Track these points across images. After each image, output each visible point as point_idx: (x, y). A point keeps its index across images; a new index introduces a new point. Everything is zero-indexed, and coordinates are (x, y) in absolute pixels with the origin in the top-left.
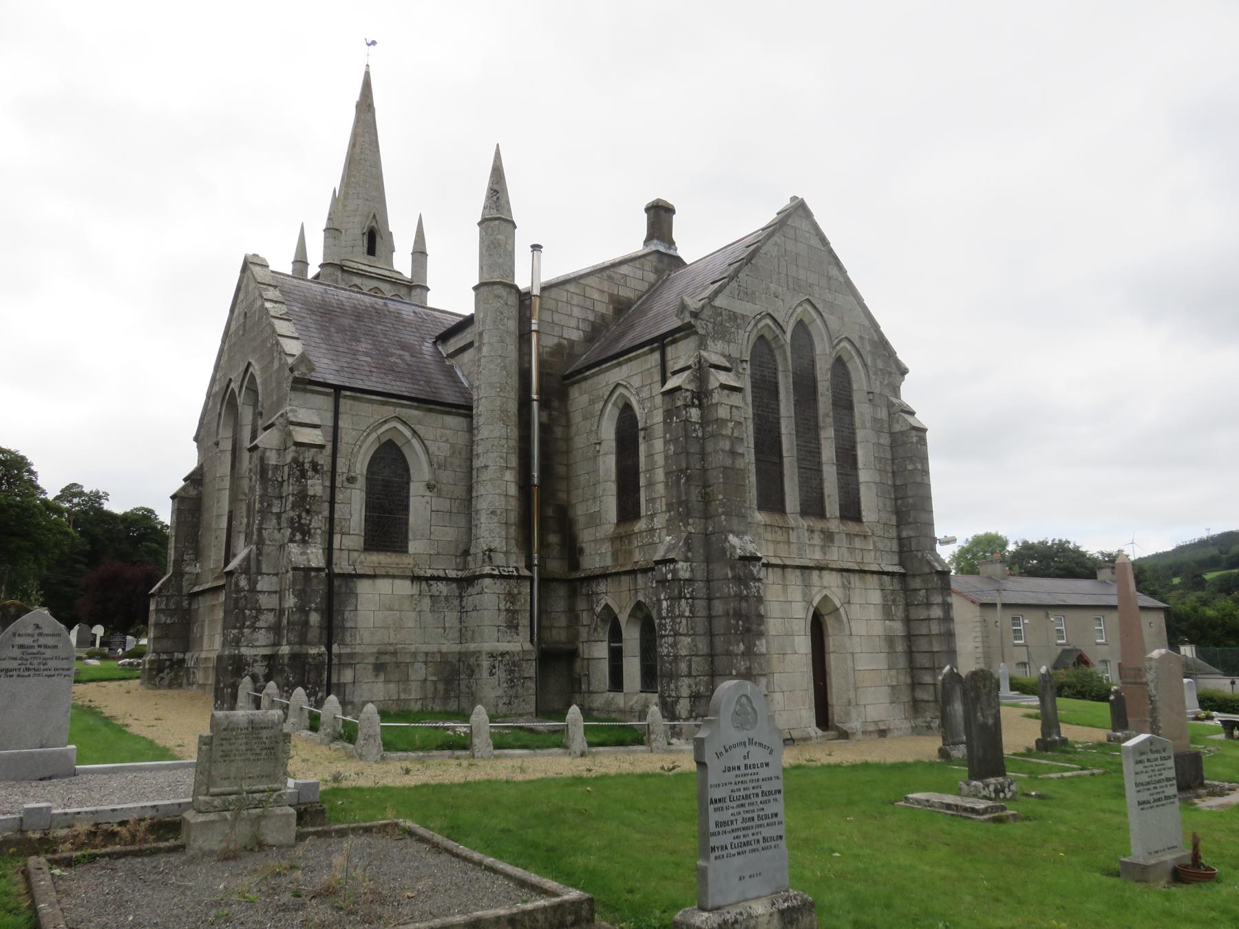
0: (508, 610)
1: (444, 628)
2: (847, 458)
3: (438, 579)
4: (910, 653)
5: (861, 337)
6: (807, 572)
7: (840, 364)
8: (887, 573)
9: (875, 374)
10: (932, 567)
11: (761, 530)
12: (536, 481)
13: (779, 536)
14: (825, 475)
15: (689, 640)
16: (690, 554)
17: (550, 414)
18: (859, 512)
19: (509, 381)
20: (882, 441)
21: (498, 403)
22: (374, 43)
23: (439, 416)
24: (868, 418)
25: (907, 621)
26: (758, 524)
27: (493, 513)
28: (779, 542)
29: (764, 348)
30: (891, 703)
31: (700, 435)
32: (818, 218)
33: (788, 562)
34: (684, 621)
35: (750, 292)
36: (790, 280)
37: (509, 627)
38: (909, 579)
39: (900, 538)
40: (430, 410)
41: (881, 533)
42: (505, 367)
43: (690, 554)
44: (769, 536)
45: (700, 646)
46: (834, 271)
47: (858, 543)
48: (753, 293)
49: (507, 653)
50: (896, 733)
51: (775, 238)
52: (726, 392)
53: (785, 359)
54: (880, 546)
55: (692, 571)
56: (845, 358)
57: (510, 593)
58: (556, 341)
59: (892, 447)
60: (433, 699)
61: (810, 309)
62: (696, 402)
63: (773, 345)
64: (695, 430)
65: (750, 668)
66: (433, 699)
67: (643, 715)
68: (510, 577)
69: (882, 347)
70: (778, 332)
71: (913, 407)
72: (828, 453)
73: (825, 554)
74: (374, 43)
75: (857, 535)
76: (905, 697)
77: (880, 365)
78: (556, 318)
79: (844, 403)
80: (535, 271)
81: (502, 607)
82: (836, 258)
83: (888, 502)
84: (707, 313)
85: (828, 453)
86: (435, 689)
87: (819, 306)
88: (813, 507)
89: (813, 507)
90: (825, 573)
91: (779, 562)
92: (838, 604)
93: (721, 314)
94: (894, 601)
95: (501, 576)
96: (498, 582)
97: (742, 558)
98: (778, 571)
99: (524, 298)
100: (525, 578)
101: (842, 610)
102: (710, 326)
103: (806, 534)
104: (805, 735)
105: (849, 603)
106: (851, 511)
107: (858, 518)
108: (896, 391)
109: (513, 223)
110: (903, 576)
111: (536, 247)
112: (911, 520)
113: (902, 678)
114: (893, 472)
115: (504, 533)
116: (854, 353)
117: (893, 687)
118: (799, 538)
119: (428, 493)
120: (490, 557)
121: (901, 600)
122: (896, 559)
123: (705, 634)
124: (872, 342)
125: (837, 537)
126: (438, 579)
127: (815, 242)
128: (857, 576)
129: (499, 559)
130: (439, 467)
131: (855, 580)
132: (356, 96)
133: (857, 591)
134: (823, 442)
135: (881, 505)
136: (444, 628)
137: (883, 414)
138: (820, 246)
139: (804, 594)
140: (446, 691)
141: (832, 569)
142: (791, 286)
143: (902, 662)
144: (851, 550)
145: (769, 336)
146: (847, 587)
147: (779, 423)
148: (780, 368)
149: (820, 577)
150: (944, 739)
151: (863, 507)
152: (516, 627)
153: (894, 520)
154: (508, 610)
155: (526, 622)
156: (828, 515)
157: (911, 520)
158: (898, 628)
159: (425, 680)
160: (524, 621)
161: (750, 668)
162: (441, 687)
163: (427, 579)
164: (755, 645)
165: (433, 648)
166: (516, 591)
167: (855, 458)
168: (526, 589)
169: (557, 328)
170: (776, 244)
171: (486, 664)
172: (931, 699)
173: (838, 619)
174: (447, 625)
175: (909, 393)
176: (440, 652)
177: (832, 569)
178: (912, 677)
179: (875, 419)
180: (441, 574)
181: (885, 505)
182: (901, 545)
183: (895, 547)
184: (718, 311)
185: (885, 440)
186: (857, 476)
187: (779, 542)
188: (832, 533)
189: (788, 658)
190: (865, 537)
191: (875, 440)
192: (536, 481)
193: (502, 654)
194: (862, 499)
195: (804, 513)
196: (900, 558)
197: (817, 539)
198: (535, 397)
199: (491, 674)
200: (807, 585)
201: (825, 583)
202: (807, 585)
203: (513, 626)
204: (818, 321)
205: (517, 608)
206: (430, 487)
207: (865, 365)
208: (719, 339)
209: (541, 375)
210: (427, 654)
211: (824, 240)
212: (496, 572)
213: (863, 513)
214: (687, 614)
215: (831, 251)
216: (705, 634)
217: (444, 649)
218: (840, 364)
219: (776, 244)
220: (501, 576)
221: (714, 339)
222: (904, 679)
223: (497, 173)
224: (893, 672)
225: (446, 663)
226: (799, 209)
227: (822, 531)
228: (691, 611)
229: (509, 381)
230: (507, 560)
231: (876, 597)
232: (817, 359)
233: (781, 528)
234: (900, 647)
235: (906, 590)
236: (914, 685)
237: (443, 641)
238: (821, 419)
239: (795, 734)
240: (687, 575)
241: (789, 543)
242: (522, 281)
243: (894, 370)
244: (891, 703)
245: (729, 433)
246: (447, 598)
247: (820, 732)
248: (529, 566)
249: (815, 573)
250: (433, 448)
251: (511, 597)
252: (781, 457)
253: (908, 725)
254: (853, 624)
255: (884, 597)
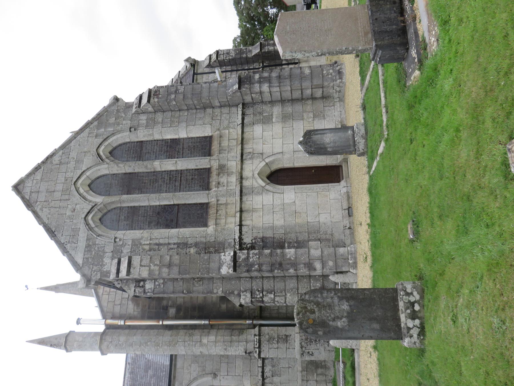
0: (278, 342)
1: (289, 367)
2: (173, 148)
3: (263, 372)
4: (293, 101)
5: (96, 136)
6: (244, 190)
7: (114, 153)
8: (243, 119)
9: (118, 124)
10: (236, 92)
11: (219, 229)
12: (207, 322)
13: (222, 212)
14: (184, 168)
15: (288, 295)
16: (236, 292)
17: (171, 306)
18: (205, 137)
19: (153, 340)
20: (160, 120)
21: (166, 347)
22: (26, 286)
23: (178, 371)
24: (146, 132)
25: (272, 102)
26: (216, 230)
27: (225, 349)
28: (226, 213)
29: (109, 218)
30: (324, 118)
31: (162, 281)
32: (23, 174)
33: (238, 209)
34: (277, 299)
35: (72, 234)
36: (64, 197)
37: (287, 341)
38: (246, 102)
39: (221, 107)
40: (174, 377)
41: (218, 122)
42: (146, 343)
43: (236, 292)
44: (223, 221)
45: (292, 285)
46: (56, 159)
47: (225, 143)
48: (73, 230)
49: (301, 343)
50: (343, 116)
51: (38, 209)
52: (132, 270)
53: (113, 203)
54: (226, 123)
55: (246, 291)
56: (110, 149)
57: (268, 341)
58: (130, 303)
59: (164, 112)
60: (326, 376)
61: (80, 181)
62: (142, 283)
63: (105, 211)
64: (159, 285)
65: (305, 264)
66: (326, 376)
67: (337, 350)
68: (260, 342)
69: (100, 119)
70: (96, 210)
71: (137, 95)
72: (169, 165)
73: (232, 172)
74: (26, 286)
75: (220, 144)
76: (320, 105)
77: (112, 120)
78: (118, 302)
79: (139, 150)
80: (93, 322)
81: (276, 346)
82: (47, 158)
83: (199, 115)
84: (87, 271)
85: (169, 165)
86: (321, 374)
87: (79, 172)
88: (202, 179)
89: (202, 179)
90: (246, 174)
91: (238, 215)
92: (263, 164)
93: (87, 258)
94: (260, 113)
95: (259, 347)
96: (263, 348)
97: (235, 270)
98: (244, 215)
99: (109, 327)
100: (260, 331)
101: (267, 160)
102: (95, 268)
103: (220, 189)
104: (345, 197)
105: (262, 154)
106: (204, 146)
107: (209, 140)
108: (129, 106)
109: (70, 332)
110: (244, 105)
111: (78, 322)
112: (208, 102)
113: (309, 108)
114: (180, 110)
115: (236, 344)
116: (106, 143)
117: (315, 117)
118: (223, 196)
119: (218, 377)
120: (250, 353)
121: (259, 108)
122: (234, 109)
123: (285, 281)
124: (98, 127)
125: (223, 162)
126: (263, 372)
127: (38, 175)
128: (245, 146)
129: (250, 347)
130: (204, 370)
131: (248, 148)
132: (53, 293)
133: (254, 146)
134: (163, 170)
135: (200, 122)
136: (289, 367)
137: (143, 118)
138: (41, 171)
139: (258, 193)
140: (322, 367)
141: (242, 169)
142: (67, 197)
143: (298, 107)
144: (230, 150)
145: (100, 215)
146: (253, 155)
147: (153, 206)
148: (119, 205)
149: (247, 179)
150: (351, 153)
151: (203, 135)
152: (287, 336)
153: (209, 111)
154: (278, 342)
155: (284, 329)
156: (208, 166)
157: (208, 102)
158: (277, 110)
159: (316, 381)
160: (283, 331)
161: (305, 264)
162: (320, 371)
163: (263, 379)
164: (290, 259)
165: (299, 375)
166: (267, 337)
167: (173, 140)
168: (265, 329)
169: (123, 302)
170: (41, 209)
171: (307, 358)
172: (321, 90)
173: (272, 162)
174: (287, 366)
175: (129, 97)
176: (301, 372)
177: (242, 169)
178: (308, 99)
179: (147, 126)
180: (260, 370)
181: (200, 118)
182: (225, 106)
183: (225, 110)
184: (86, 260)
185: (159, 117)
186: (183, 139)
187: (226, 213)
188: (219, 165)
189: (298, 209)
190: (221, 137)
191: (160, 125)
192: (207, 322)
193: (302, 347)
194: (198, 136)
195: (207, 187)
196: (233, 106)
197: (223, 179)
198: (161, 323)
199: (312, 355)
200: (253, 191)
201: (250, 175)
202: (253, 191)
203: (286, 339)
204: (88, 173)
205: (276, 337)
206: (215, 375)
207: (113, 134)
208: (103, 261)
209: (150, 318)
210: (303, 380)
211: (37, 168)
212: (257, 350)
213: (206, 135)
214: (272, 296)
215: (43, 162)
216: (285, 281)
217: (300, 369)
218: (114, 153)
219: (41, 209)
220: (259, 347)
221: (103, 265)
222: (309, 106)
223: (42, 342)
224: (305, 115)
225: (307, 368)
226: (17, 188)
227: (218, 175)
228: (271, 293)
229: (153, 340)
230: (250, 341)
231: (258, 129)
232: (112, 173)
233: (217, 211)
234: (289, 109)
235: (253, 103)
236: (313, 98)
237: (295, 368)
238: (149, 171)
239: (345, 206)
240: (249, 295)
241: (226, 204)
242: (101, 328)
243: (115, 108)
244: (324, 118)
245: (157, 268)
246: (273, 366)
247: (343, 183)
248: (254, 326)
249: (246, 183)
250: (194, 374)
251: (270, 339)
252: (174, 205)
253: (338, 104)
254: (275, 151)
255: (258, 122)
